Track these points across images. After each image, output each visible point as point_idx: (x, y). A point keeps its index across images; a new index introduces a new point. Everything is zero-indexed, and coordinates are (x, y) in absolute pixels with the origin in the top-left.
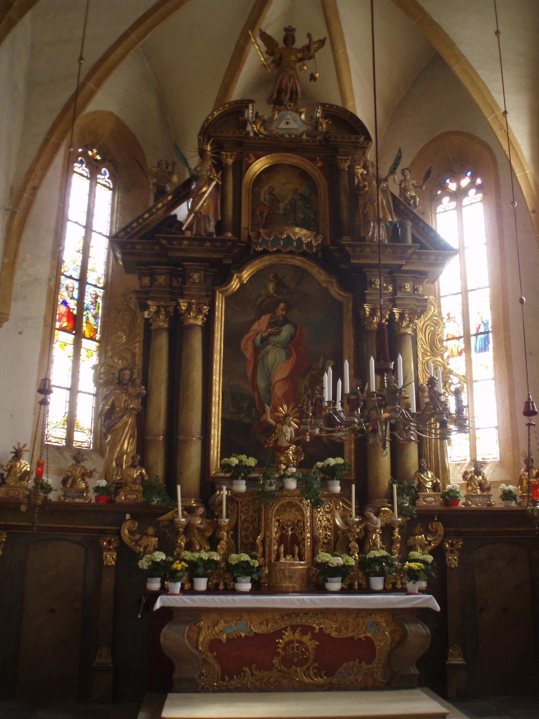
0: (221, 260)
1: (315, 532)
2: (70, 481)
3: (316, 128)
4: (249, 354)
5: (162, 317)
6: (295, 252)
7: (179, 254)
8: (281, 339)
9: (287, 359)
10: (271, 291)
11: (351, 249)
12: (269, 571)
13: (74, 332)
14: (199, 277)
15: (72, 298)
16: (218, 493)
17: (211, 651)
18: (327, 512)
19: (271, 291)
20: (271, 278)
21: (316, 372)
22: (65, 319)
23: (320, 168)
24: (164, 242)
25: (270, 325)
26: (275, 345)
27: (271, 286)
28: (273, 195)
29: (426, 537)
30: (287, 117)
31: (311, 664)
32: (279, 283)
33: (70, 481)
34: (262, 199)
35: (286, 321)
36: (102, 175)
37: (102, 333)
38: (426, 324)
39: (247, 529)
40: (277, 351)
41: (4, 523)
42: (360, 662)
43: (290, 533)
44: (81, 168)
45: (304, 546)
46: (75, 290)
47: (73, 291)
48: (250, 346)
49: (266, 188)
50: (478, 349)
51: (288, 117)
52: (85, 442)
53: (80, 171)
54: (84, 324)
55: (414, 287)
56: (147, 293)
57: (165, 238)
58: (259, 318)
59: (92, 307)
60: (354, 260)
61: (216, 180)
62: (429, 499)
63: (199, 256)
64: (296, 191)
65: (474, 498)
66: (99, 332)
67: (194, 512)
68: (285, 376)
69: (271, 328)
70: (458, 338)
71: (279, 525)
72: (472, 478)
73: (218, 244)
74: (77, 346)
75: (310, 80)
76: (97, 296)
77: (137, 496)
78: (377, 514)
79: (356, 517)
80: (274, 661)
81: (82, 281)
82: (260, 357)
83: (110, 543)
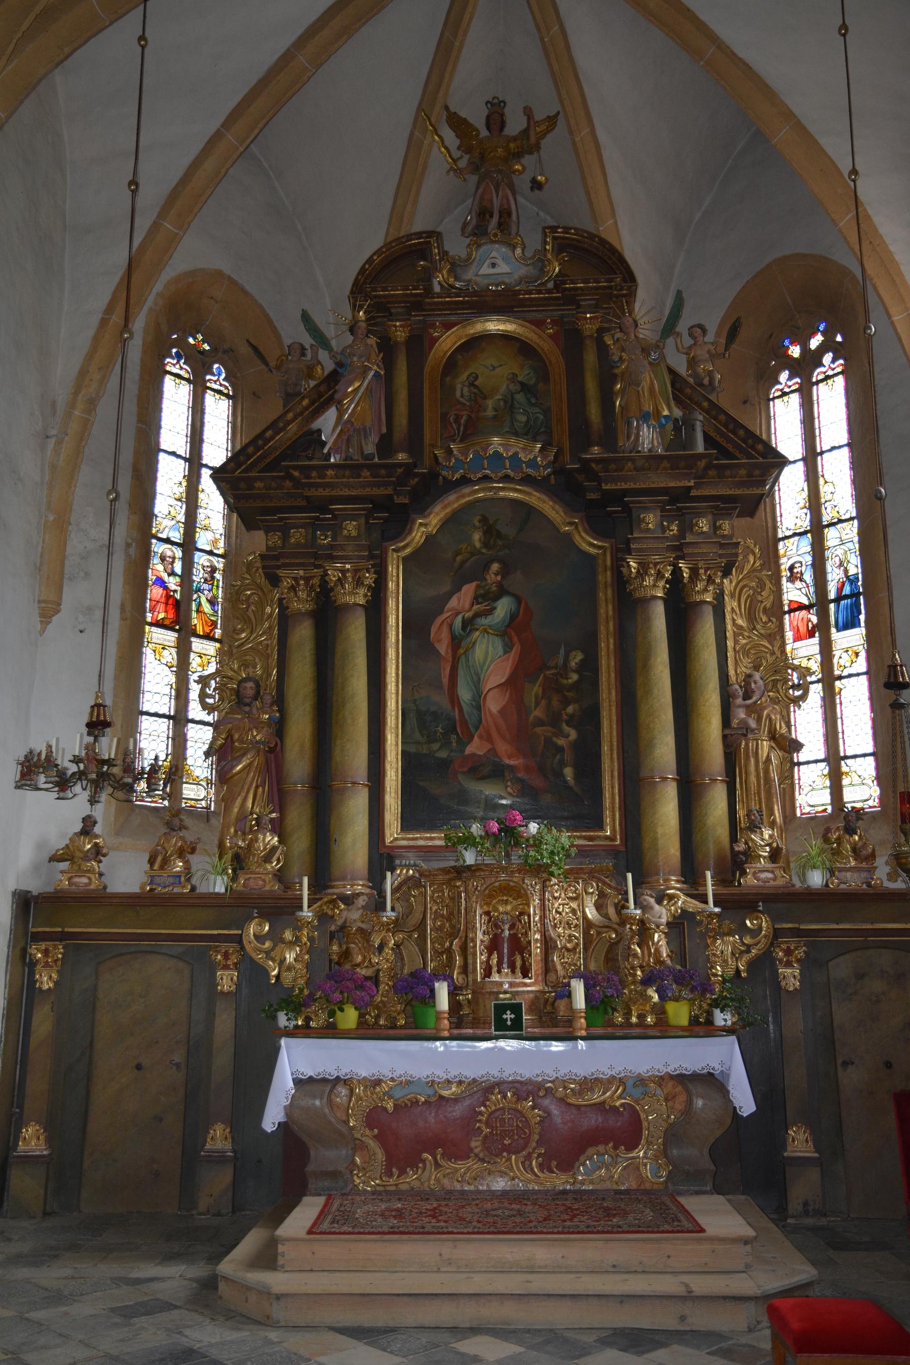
0: (390, 497)
1: (548, 931)
2: (159, 859)
3: (542, 270)
4: (443, 648)
5: (302, 595)
6: (513, 478)
7: (321, 492)
8: (496, 621)
9: (505, 652)
10: (478, 545)
11: (600, 466)
12: (473, 996)
13: (177, 627)
14: (358, 528)
15: (172, 574)
16: (398, 872)
17: (370, 1127)
18: (571, 899)
19: (478, 545)
20: (477, 524)
21: (554, 671)
22: (161, 607)
23: (551, 336)
24: (296, 474)
25: (476, 599)
26: (485, 631)
27: (477, 537)
28: (476, 387)
29: (741, 939)
30: (492, 255)
31: (534, 1149)
32: (490, 531)
33: (159, 859)
34: (458, 394)
35: (502, 592)
36: (214, 375)
37: (223, 628)
38: (741, 584)
39: (440, 929)
40: (488, 640)
41: (60, 929)
42: (615, 1148)
43: (507, 933)
44: (178, 366)
45: (530, 955)
46: (177, 561)
47: (173, 562)
48: (445, 635)
49: (464, 377)
50: (841, 623)
51: (494, 254)
52: (202, 800)
53: (175, 370)
54: (194, 615)
55: (715, 524)
56: (276, 558)
57: (296, 468)
58: (459, 590)
59: (206, 586)
60: (606, 484)
61: (375, 367)
62: (763, 875)
63: (354, 493)
64: (513, 378)
65: (843, 873)
66: (219, 626)
67: (353, 903)
68: (503, 680)
69: (478, 603)
70: (807, 608)
71: (489, 921)
72: (839, 840)
73: (383, 472)
74: (183, 650)
75: (532, 189)
76: (214, 569)
77: (89, 878)
78: (659, 902)
79: (635, 908)
80: (473, 1144)
81: (188, 545)
82: (461, 651)
83: (226, 956)
